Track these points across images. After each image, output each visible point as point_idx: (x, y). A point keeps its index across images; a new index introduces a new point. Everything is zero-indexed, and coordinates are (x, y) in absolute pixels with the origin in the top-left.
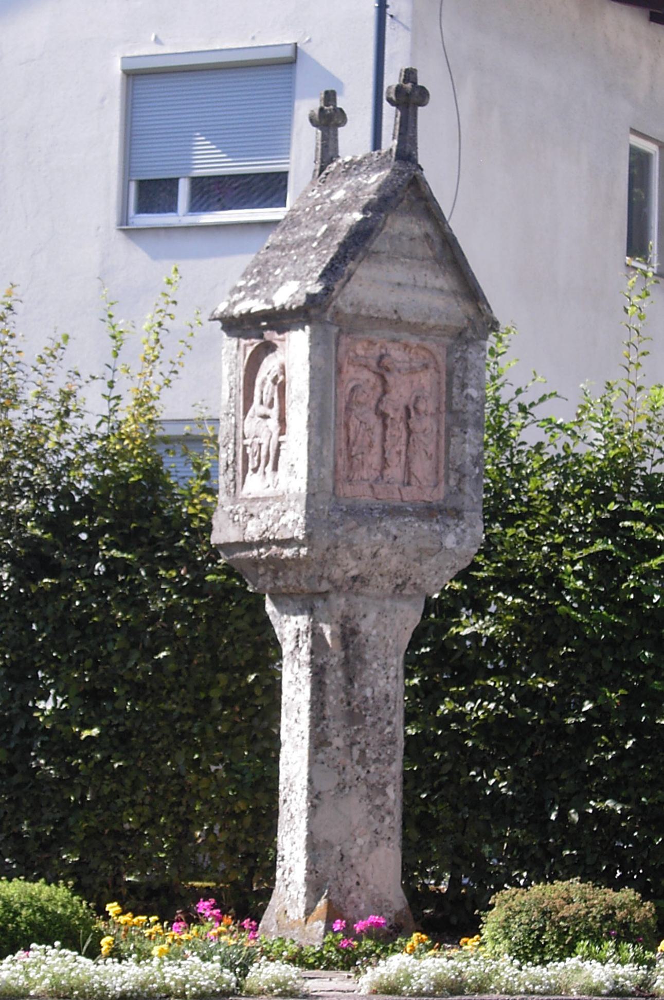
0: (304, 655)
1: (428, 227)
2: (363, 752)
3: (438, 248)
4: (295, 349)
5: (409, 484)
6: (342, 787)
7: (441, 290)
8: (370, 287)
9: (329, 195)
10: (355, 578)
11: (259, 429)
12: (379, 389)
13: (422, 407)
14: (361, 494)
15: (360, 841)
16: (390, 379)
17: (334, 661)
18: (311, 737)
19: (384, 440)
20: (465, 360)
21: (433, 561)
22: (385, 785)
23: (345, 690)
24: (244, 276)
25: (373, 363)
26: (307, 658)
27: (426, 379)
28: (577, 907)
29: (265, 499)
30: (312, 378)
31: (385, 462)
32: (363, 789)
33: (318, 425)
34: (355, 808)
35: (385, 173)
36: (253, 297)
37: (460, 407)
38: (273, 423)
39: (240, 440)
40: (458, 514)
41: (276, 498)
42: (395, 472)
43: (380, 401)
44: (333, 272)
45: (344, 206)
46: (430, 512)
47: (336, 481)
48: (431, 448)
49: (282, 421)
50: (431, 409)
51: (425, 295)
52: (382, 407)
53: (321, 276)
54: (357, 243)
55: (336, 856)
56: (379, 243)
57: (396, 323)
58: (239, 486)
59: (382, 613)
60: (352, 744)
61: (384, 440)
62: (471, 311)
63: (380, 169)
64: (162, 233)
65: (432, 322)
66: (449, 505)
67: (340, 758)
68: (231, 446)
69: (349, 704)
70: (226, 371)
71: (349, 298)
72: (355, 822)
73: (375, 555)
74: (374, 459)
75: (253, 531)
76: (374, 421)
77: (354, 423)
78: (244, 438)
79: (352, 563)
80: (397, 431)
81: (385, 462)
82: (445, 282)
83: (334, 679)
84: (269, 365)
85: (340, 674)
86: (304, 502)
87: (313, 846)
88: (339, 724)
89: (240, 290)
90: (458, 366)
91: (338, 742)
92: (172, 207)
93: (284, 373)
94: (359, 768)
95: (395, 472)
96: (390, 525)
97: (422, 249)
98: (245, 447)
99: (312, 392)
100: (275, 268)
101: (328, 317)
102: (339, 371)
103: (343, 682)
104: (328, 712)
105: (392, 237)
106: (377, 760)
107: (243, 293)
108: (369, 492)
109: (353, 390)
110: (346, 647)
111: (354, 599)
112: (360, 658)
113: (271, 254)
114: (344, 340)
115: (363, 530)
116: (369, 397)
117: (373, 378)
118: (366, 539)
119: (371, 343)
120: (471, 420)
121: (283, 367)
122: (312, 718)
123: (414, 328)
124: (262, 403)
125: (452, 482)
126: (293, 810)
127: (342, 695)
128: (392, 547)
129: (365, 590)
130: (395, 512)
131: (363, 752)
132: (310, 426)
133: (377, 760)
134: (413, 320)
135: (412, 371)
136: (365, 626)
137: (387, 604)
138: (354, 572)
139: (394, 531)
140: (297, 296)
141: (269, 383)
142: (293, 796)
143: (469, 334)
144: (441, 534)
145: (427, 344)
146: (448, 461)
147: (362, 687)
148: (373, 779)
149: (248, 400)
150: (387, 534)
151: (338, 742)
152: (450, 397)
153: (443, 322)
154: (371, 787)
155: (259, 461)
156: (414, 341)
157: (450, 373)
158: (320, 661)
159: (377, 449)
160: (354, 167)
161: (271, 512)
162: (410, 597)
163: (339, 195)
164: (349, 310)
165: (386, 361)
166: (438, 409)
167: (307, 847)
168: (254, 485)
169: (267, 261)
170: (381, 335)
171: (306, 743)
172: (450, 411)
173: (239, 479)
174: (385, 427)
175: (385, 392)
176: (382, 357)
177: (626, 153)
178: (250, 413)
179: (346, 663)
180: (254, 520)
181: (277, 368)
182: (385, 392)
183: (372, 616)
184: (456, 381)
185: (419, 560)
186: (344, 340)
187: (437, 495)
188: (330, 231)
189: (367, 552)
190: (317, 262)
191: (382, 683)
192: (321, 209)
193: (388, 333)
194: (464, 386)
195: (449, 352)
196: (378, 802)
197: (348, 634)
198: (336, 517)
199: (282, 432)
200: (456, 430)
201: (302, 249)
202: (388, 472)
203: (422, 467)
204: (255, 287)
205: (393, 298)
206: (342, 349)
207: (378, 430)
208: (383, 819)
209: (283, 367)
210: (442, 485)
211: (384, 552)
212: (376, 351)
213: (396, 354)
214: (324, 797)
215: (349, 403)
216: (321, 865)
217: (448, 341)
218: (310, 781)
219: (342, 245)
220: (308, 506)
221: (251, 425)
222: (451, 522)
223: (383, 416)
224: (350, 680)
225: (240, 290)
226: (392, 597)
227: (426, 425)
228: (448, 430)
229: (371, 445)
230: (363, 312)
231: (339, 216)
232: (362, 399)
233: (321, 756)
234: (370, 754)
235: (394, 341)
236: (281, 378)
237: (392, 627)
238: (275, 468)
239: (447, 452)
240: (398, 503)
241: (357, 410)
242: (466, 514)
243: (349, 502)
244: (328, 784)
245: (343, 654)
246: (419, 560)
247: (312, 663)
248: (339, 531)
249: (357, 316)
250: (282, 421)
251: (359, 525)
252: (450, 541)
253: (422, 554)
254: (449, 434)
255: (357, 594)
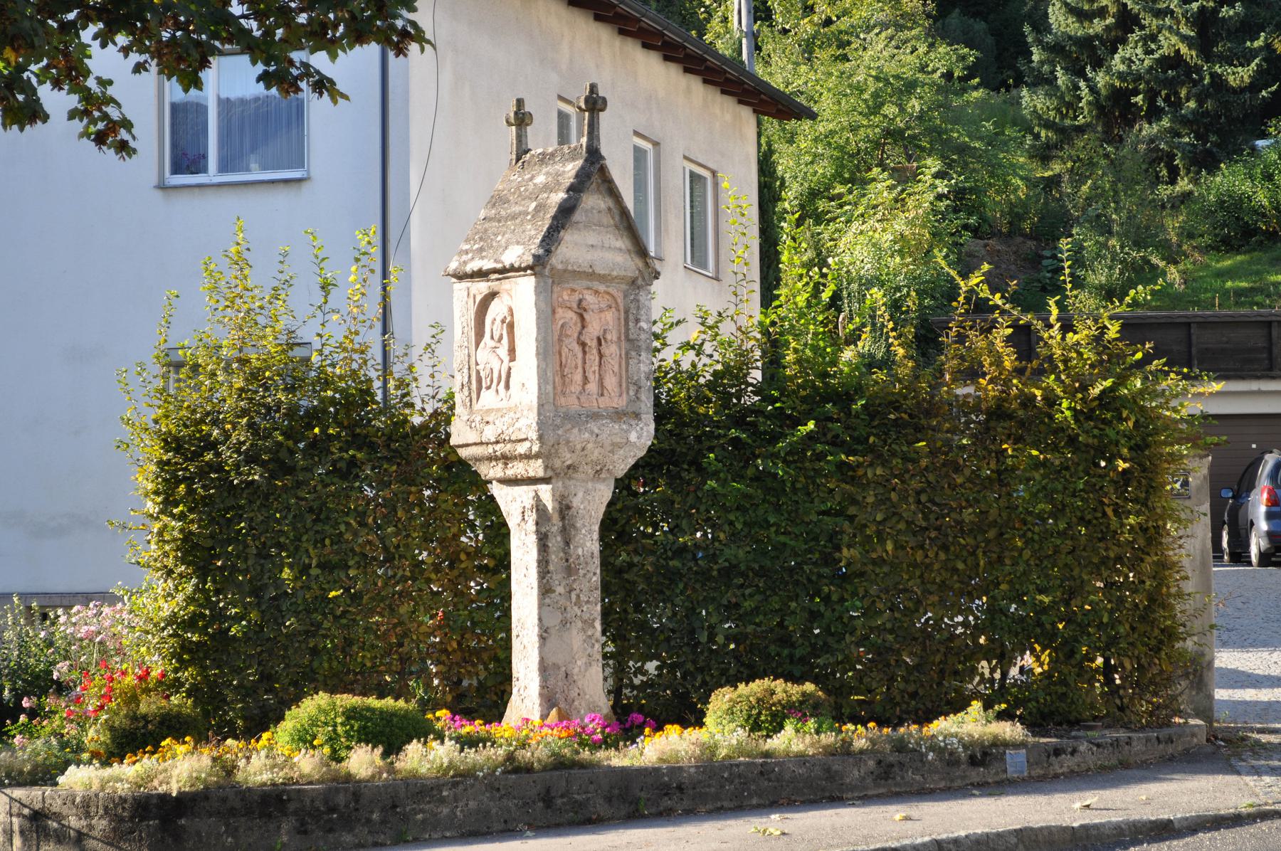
0: (531, 526)
1: (610, 202)
2: (578, 596)
3: (617, 218)
4: (521, 296)
5: (602, 395)
6: (565, 623)
7: (620, 249)
8: (577, 248)
9: (531, 179)
10: (569, 467)
11: (489, 358)
12: (579, 325)
13: (609, 337)
14: (571, 403)
15: (579, 663)
16: (586, 316)
17: (554, 529)
18: (539, 587)
19: (584, 362)
20: (638, 301)
21: (622, 452)
22: (594, 620)
23: (563, 550)
24: (467, 241)
25: (575, 306)
26: (534, 528)
27: (610, 316)
28: (780, 695)
29: (498, 410)
30: (538, 318)
31: (586, 380)
32: (580, 624)
33: (544, 352)
34: (576, 638)
35: (579, 163)
36: (482, 258)
37: (635, 336)
38: (503, 351)
39: (473, 366)
40: (637, 416)
41: (510, 409)
42: (592, 387)
43: (580, 333)
44: (551, 238)
45: (547, 188)
46: (618, 415)
47: (555, 394)
48: (616, 369)
49: (512, 351)
50: (615, 339)
51: (611, 254)
52: (582, 338)
53: (543, 241)
54: (565, 213)
55: (562, 674)
56: (578, 216)
57: (592, 275)
58: (474, 401)
59: (587, 492)
60: (570, 592)
61: (584, 362)
62: (640, 264)
63: (574, 159)
64: (197, 190)
65: (615, 273)
66: (630, 409)
67: (562, 601)
68: (466, 371)
69: (567, 560)
70: (457, 314)
71: (560, 258)
72: (575, 649)
73: (583, 449)
74: (578, 377)
75: (490, 434)
76: (578, 349)
77: (565, 351)
78: (477, 364)
79: (568, 456)
80: (593, 356)
81: (586, 380)
82: (622, 243)
83: (555, 542)
84: (496, 310)
85: (559, 539)
86: (535, 411)
87: (544, 669)
88: (559, 576)
89: (467, 252)
90: (632, 306)
91: (560, 589)
92: (203, 169)
93: (512, 315)
94: (576, 608)
95: (592, 387)
96: (593, 426)
97: (607, 220)
98: (478, 372)
99: (538, 328)
100: (496, 235)
101: (547, 272)
102: (554, 312)
103: (561, 544)
104: (551, 568)
105: (586, 211)
106: (588, 602)
107: (470, 255)
108: (576, 402)
109: (562, 326)
110: (563, 518)
111: (567, 482)
112: (573, 526)
113: (487, 225)
114: (556, 289)
115: (575, 431)
116: (573, 331)
117: (575, 317)
118: (578, 437)
119: (573, 290)
120: (644, 346)
121: (511, 310)
122: (539, 572)
123: (603, 278)
124: (492, 338)
125: (632, 393)
126: (525, 642)
127: (562, 554)
128: (595, 442)
129: (575, 475)
130: (595, 416)
131: (578, 596)
132: (538, 354)
133: (588, 602)
134: (602, 272)
135: (601, 311)
136: (576, 502)
137: (590, 485)
138: (569, 463)
139: (596, 431)
140: (525, 258)
141: (498, 322)
142: (524, 632)
143: (640, 282)
144: (627, 431)
145: (610, 290)
146: (628, 378)
147: (576, 547)
148: (586, 616)
149: (480, 334)
150: (592, 432)
151: (560, 589)
152: (627, 330)
153: (623, 273)
154: (585, 622)
155: (492, 381)
156: (602, 288)
157: (627, 312)
158: (543, 530)
159: (580, 370)
160: (544, 159)
161: (506, 419)
162: (604, 480)
163: (541, 179)
164: (560, 267)
165: (584, 304)
166: (619, 338)
167: (540, 669)
168: (488, 399)
169: (486, 230)
170: (579, 284)
171: (535, 591)
172: (628, 339)
173: (474, 396)
174: (584, 353)
175: (583, 327)
176: (580, 301)
177: (555, 115)
178: (482, 345)
179: (564, 530)
180: (491, 427)
181: (505, 312)
182: (583, 327)
183: (580, 494)
184: (631, 317)
185: (612, 452)
186: (556, 289)
187: (620, 403)
188: (540, 208)
189: (579, 447)
190: (535, 232)
191: (588, 544)
192: (526, 190)
193: (585, 283)
194: (637, 321)
195: (625, 296)
196: (590, 633)
197: (565, 509)
198: (558, 421)
199: (513, 359)
200: (633, 353)
201: (518, 221)
202: (588, 386)
203: (611, 382)
204: (481, 249)
205: (589, 257)
206: (555, 296)
207: (580, 355)
208: (593, 646)
209: (511, 310)
210: (625, 395)
211: (590, 446)
212: (576, 297)
213: (590, 298)
214: (553, 631)
215: (560, 335)
216: (551, 682)
217: (624, 287)
218: (540, 619)
219: (554, 218)
220: (539, 414)
221: (483, 355)
222: (633, 422)
223: (583, 345)
224: (567, 544)
225: (467, 252)
226: (592, 480)
227: (611, 350)
228: (627, 354)
229: (576, 367)
230: (570, 268)
231: (545, 195)
232: (569, 333)
233: (547, 601)
234: (583, 598)
235: (588, 288)
236: (508, 319)
237: (593, 501)
238: (507, 387)
239: (627, 371)
240: (596, 410)
241: (567, 341)
242: (643, 416)
243: (564, 410)
244: (554, 621)
245: (560, 524)
246: (612, 452)
247: (537, 532)
248: (560, 432)
249: (565, 271)
250: (512, 351)
251: (573, 427)
252: (633, 437)
253: (616, 446)
254: (628, 357)
255: (570, 478)
